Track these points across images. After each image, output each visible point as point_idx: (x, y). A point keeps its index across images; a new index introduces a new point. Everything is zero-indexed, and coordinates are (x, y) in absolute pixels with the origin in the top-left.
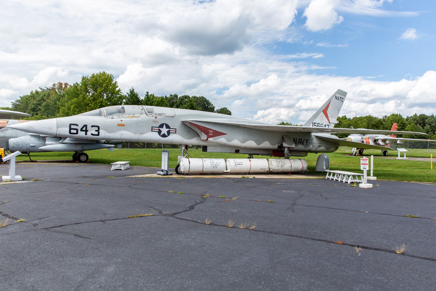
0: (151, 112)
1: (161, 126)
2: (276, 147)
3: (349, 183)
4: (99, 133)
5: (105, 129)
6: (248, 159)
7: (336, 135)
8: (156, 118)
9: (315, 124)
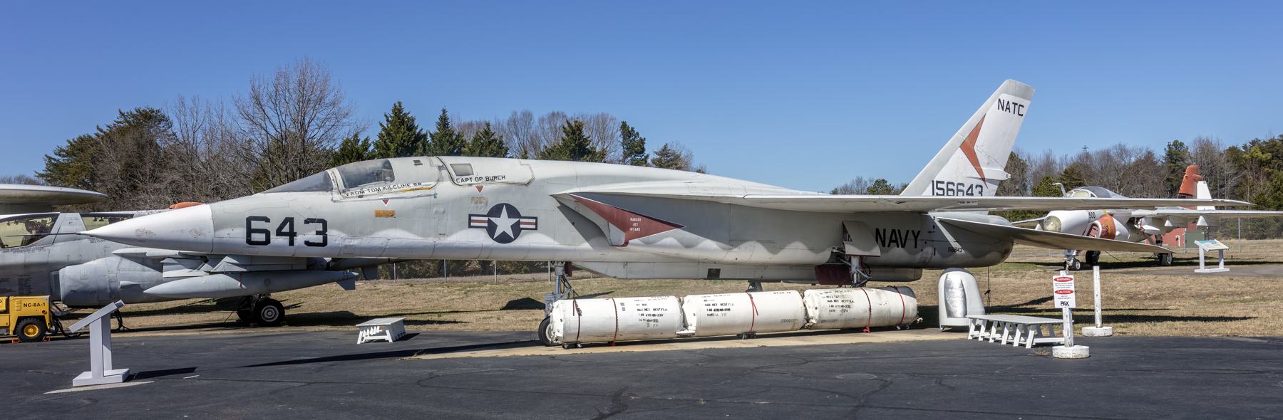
0: (465, 173)
1: (496, 211)
2: (824, 257)
3: (1028, 346)
4: (325, 239)
5: (341, 228)
6: (745, 295)
7: (1002, 214)
8: (480, 189)
9: (940, 185)
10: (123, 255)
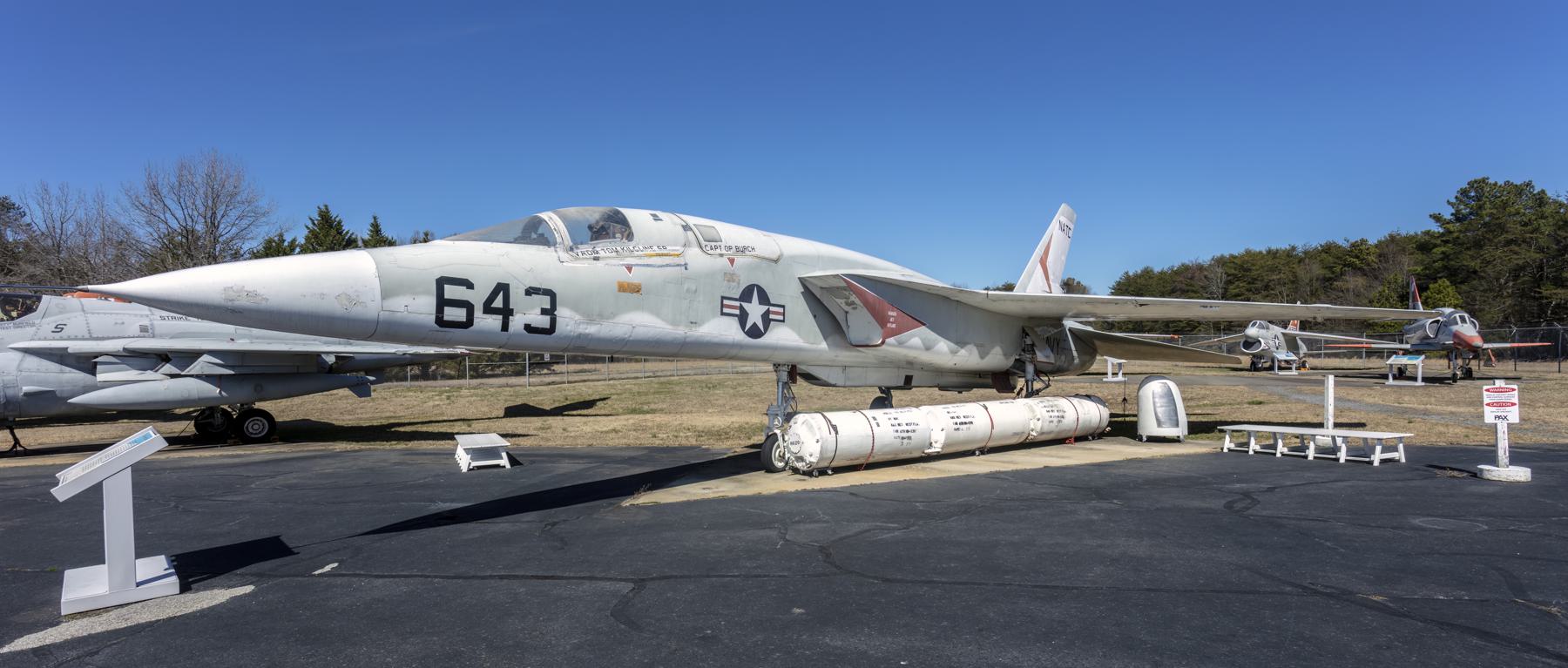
1: (746, 295)
8: (732, 261)
10: (27, 351)
